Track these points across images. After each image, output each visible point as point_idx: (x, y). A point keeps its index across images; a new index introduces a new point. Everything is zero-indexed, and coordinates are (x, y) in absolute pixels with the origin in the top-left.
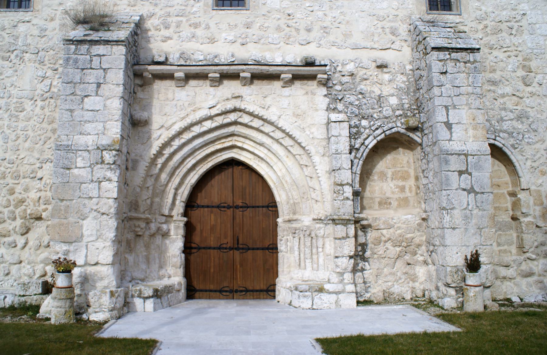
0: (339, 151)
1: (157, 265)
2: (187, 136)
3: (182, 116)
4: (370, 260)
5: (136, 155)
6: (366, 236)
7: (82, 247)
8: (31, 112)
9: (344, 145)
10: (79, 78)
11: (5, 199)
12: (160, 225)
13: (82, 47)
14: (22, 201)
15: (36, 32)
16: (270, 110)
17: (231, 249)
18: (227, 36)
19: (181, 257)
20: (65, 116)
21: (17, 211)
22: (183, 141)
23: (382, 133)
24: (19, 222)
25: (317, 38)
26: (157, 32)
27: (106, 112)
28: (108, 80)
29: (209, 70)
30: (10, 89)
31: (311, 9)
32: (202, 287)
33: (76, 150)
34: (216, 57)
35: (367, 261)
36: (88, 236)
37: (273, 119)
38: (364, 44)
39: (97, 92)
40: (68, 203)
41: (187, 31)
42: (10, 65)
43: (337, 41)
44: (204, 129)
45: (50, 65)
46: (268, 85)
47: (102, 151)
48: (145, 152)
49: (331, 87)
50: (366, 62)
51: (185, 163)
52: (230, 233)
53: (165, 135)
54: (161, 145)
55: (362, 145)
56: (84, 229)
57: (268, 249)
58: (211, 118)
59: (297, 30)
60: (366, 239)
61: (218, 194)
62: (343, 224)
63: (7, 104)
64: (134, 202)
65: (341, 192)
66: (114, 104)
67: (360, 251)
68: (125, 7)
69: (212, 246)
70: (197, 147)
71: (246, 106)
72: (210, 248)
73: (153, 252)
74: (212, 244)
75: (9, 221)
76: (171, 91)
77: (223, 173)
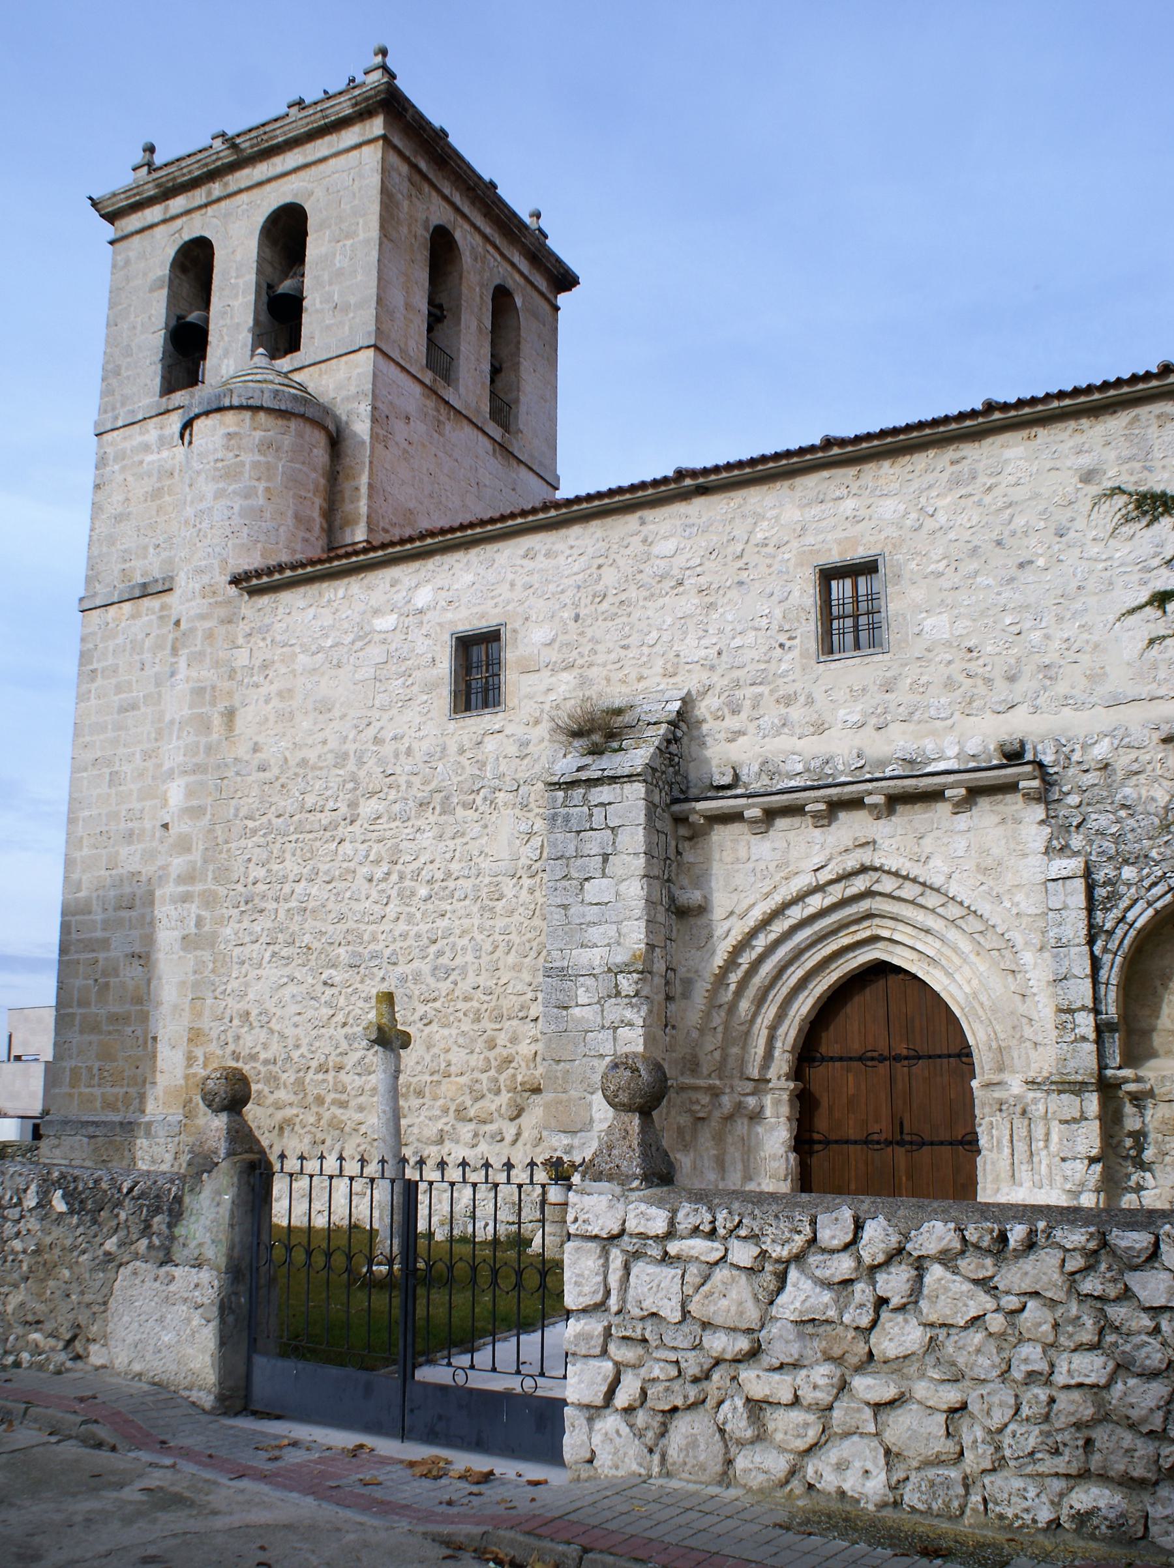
0: (1064, 940)
1: (739, 1175)
2: (779, 927)
3: (765, 890)
4: (1154, 1167)
5: (688, 971)
6: (1142, 1115)
7: (592, 1139)
8: (514, 900)
9: (1075, 926)
10: (573, 849)
11: (482, 1056)
12: (742, 1099)
13: (574, 793)
14: (508, 1061)
15: (513, 750)
16: (931, 864)
17: (889, 1143)
18: (848, 714)
19: (787, 1159)
20: (556, 917)
21: (502, 1078)
22: (773, 936)
23: (1167, 893)
24: (505, 1097)
25: (1029, 694)
26: (718, 722)
27: (619, 905)
28: (619, 847)
29: (804, 799)
30: (479, 860)
31: (1016, 629)
32: (374, 1121)
33: (576, 976)
34: (827, 763)
35: (1150, 1170)
36: (601, 1121)
37: (937, 881)
38: (1132, 692)
39: (603, 870)
40: (568, 1066)
41: (771, 715)
42: (476, 816)
43: (1074, 692)
44: (810, 911)
45: (537, 810)
46: (925, 812)
47: (616, 974)
48: (703, 964)
49: (1059, 801)
50: (1138, 734)
51: (785, 977)
52: (885, 1112)
53: (738, 929)
54: (730, 949)
55: (1118, 923)
56: (594, 1109)
57: (961, 1143)
58: (819, 889)
59: (988, 681)
60: (1143, 1122)
61: (860, 1032)
62: (1072, 1092)
63: (476, 888)
64: (688, 1057)
65: (1070, 1026)
66: (631, 889)
67: (1131, 1148)
68: (658, 679)
69: (852, 1138)
70: (803, 946)
71: (883, 861)
72: (847, 1142)
73: (731, 1149)
74: (852, 1134)
75: (489, 1096)
76: (743, 843)
77: (868, 991)
